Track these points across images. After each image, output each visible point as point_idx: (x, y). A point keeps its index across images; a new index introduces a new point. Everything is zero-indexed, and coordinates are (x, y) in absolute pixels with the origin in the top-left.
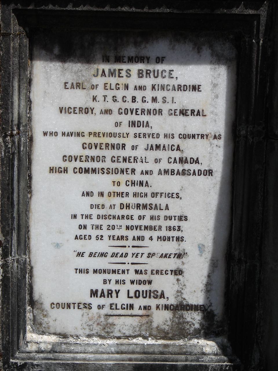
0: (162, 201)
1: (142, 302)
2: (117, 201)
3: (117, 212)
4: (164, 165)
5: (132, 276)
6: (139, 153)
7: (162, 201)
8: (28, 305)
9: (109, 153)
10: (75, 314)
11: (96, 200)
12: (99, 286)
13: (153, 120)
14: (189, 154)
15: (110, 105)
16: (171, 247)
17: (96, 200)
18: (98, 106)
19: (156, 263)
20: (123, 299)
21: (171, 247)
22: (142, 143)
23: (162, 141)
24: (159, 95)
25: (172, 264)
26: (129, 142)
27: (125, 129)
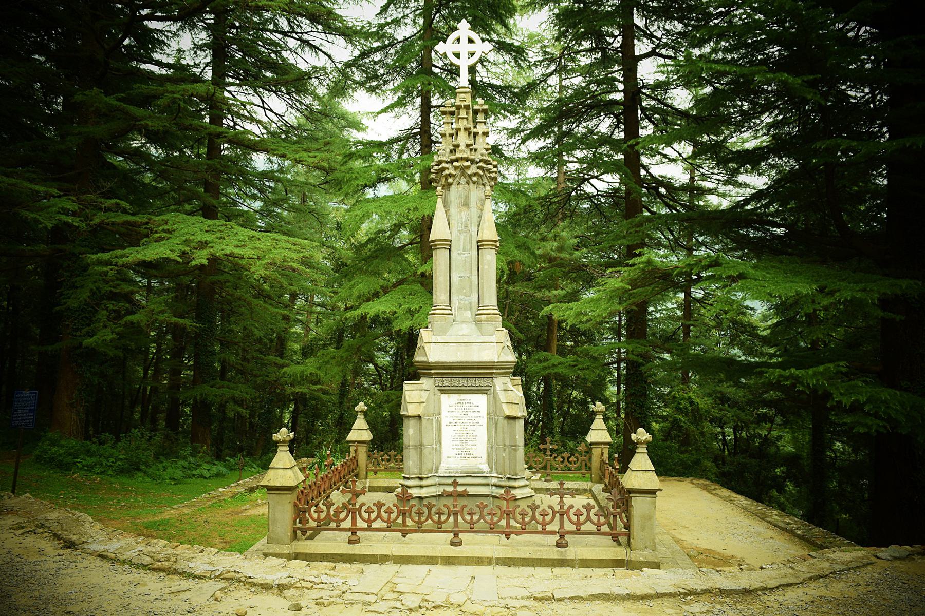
19: (470, 447)
20: (463, 456)
22: (466, 419)
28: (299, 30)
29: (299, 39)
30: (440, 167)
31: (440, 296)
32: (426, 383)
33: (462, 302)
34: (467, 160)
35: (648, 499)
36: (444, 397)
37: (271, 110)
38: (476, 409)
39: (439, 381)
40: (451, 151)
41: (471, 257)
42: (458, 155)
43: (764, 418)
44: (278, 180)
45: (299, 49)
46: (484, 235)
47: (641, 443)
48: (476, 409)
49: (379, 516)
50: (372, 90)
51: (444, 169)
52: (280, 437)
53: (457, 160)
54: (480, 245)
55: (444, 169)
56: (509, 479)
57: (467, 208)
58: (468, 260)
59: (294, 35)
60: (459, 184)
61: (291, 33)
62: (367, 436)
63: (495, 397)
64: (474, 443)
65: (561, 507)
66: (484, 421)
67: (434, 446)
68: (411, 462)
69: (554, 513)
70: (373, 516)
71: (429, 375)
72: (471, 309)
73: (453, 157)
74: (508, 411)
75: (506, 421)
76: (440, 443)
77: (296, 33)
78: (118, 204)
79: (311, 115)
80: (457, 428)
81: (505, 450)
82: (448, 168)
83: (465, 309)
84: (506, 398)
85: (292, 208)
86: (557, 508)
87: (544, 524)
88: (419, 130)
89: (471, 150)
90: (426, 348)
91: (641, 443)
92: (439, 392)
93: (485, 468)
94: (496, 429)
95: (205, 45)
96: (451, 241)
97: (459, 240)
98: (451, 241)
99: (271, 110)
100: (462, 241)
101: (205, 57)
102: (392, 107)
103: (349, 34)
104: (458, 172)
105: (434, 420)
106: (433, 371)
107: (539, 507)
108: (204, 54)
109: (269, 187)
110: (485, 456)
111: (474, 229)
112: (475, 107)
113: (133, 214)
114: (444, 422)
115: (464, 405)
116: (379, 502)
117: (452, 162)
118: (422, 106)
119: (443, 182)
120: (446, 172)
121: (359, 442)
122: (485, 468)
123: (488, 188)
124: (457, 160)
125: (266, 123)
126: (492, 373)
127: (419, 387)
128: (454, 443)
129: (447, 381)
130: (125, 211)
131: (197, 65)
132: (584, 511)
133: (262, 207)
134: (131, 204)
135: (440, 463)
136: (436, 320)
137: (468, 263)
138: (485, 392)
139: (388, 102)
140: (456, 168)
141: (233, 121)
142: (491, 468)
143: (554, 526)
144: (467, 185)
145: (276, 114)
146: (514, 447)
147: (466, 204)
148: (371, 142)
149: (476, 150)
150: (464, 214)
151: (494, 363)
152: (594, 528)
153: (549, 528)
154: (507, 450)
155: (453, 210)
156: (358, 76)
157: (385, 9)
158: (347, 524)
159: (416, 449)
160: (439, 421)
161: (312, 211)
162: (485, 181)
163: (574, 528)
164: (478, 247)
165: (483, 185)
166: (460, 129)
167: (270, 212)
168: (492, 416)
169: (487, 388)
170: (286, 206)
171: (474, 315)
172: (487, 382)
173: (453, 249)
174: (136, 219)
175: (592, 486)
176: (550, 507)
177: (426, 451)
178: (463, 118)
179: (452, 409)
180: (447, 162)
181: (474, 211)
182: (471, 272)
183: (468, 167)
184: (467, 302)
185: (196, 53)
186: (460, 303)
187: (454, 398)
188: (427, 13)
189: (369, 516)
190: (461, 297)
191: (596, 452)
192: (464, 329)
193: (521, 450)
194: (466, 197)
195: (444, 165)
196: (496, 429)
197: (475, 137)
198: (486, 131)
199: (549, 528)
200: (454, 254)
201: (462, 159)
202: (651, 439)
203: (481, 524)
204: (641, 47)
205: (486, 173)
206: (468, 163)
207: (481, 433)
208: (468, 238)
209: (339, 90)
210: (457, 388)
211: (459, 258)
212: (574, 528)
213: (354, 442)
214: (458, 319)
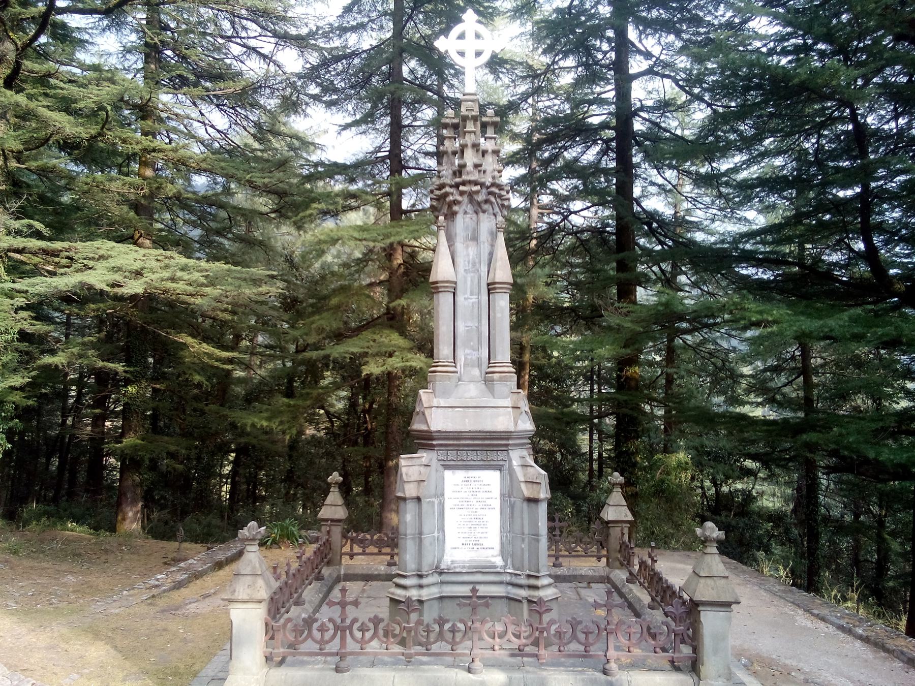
20: (471, 546)
22: (475, 500)
28: (244, 34)
29: (244, 46)
30: (443, 191)
31: (443, 350)
32: (424, 456)
33: (469, 357)
34: (476, 183)
35: (721, 614)
36: (448, 474)
37: (212, 126)
39: (442, 454)
40: (454, 173)
41: (479, 303)
42: (465, 177)
43: (749, 473)
44: (222, 206)
45: (245, 57)
46: (497, 276)
47: (711, 541)
50: (330, 104)
51: (447, 194)
52: (247, 534)
53: (464, 183)
54: (491, 288)
55: (447, 194)
56: (529, 576)
57: (475, 243)
58: (476, 306)
59: (238, 40)
60: (465, 213)
61: (234, 37)
62: (341, 513)
63: (511, 472)
64: (484, 530)
66: (496, 503)
67: (436, 534)
68: (408, 556)
71: (431, 447)
72: (479, 366)
73: (458, 180)
74: (527, 491)
75: (525, 504)
76: (444, 531)
77: (241, 38)
78: (30, 226)
79: (262, 133)
80: (464, 512)
81: (523, 540)
82: (452, 194)
83: (473, 366)
84: (525, 476)
85: (237, 239)
89: (480, 171)
90: (426, 413)
91: (711, 541)
92: (441, 468)
93: (499, 561)
94: (512, 513)
95: (135, 48)
96: (455, 283)
97: (465, 282)
98: (455, 283)
99: (212, 126)
100: (469, 283)
101: (136, 61)
102: (356, 123)
103: (301, 42)
104: (465, 199)
105: (436, 502)
106: (434, 443)
107: (580, 622)
108: (135, 59)
109: (210, 214)
110: (497, 547)
111: (484, 269)
112: (484, 119)
113: (50, 239)
114: (448, 504)
115: (473, 483)
116: (376, 617)
117: (457, 186)
118: (391, 124)
119: (445, 210)
120: (451, 198)
121: (332, 520)
122: (499, 561)
123: (500, 219)
124: (464, 183)
126: (507, 445)
127: (417, 462)
129: (452, 455)
130: (38, 235)
131: (127, 70)
133: (201, 236)
134: (46, 227)
135: (443, 556)
136: (439, 382)
137: (476, 310)
138: (499, 468)
139: (349, 120)
140: (462, 193)
141: (168, 137)
142: (505, 561)
144: (475, 215)
145: (219, 131)
146: (536, 536)
147: (475, 238)
148: (335, 164)
149: (484, 172)
150: (472, 251)
151: (511, 432)
154: (527, 540)
155: (459, 246)
156: (314, 89)
157: (348, 10)
159: (413, 539)
160: (442, 504)
161: (261, 243)
162: (497, 209)
164: (489, 290)
165: (495, 215)
166: (466, 146)
167: (212, 242)
168: (507, 496)
169: (501, 463)
170: (230, 236)
171: (483, 373)
172: (502, 455)
173: (458, 292)
174: (58, 245)
175: (610, 573)
176: (330, 620)
177: (426, 543)
178: (470, 132)
179: (458, 488)
180: (451, 186)
181: (485, 249)
182: (480, 321)
183: (477, 192)
184: (475, 358)
185: (124, 56)
186: (466, 359)
187: (461, 474)
188: (399, 17)
190: (468, 351)
191: (615, 532)
192: (472, 391)
193: (544, 542)
194: (474, 230)
195: (448, 189)
196: (512, 513)
197: (483, 156)
198: (496, 148)
200: (460, 298)
201: (470, 182)
202: (724, 537)
204: (637, 64)
205: (499, 200)
206: (478, 188)
207: (493, 519)
208: (476, 281)
209: (291, 106)
210: (464, 463)
211: (466, 303)
213: (327, 520)
214: (464, 378)
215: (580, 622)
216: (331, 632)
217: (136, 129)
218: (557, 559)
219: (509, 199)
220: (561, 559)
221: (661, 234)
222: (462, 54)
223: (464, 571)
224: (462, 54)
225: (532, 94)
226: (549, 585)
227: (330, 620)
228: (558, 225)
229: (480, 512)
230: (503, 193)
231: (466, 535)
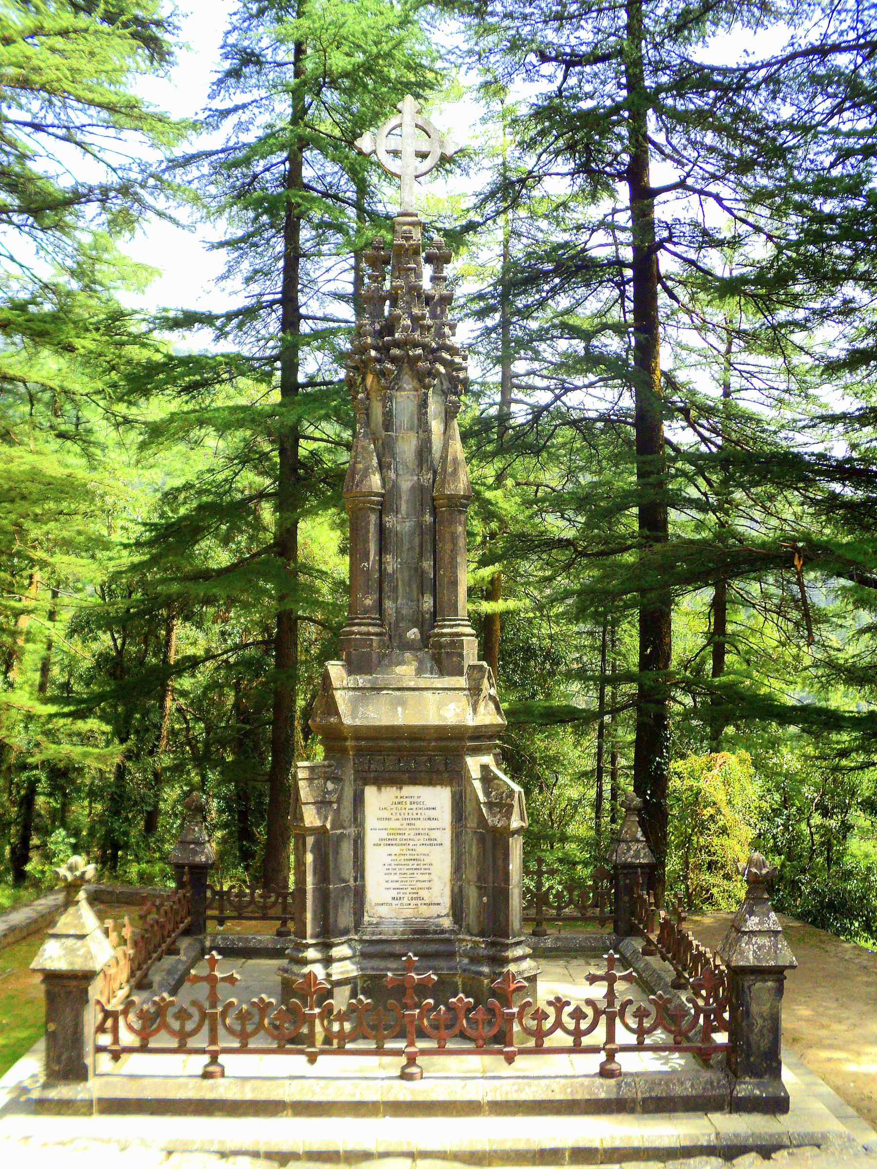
0: (422, 857)
1: (414, 902)
2: (403, 857)
3: (403, 862)
4: (422, 842)
5: (410, 890)
6: (412, 837)
7: (422, 857)
8: (320, 737)
9: (398, 837)
10: (386, 908)
11: (393, 857)
12: (396, 896)
13: (417, 823)
14: (433, 837)
15: (398, 817)
16: (426, 877)
17: (393, 857)
18: (394, 817)
19: (419, 885)
20: (406, 901)
21: (426, 877)
22: (412, 832)
23: (421, 831)
24: (419, 812)
25: (427, 885)
26: (407, 832)
27: (405, 826)
38: (432, 814)
48: (432, 814)
49: (558, 1024)
65: (611, 1004)
69: (598, 1013)
70: (548, 1024)
80: (396, 850)
86: (602, 1005)
87: (577, 1034)
88: (280, 296)
114: (371, 838)
125: (792, 332)
128: (387, 877)
132: (551, 1011)
143: (598, 1036)
152: (569, 1041)
153: (586, 1041)
158: (598, 1036)
163: (632, 1039)
176: (194, 1003)
179: (386, 814)
187: (390, 793)
189: (578, 1024)
199: (586, 1041)
203: (561, 1039)
212: (632, 1039)
215: (568, 1003)
216: (196, 1017)
217: (306, 126)
218: (539, 924)
219: (465, 369)
220: (545, 925)
221: (702, 426)
222: (396, 153)
223: (395, 938)
224: (396, 153)
225: (840, 313)
226: (472, 635)
227: (194, 1003)
228: (546, 407)
229: (420, 849)
230: (458, 359)
231: (397, 885)
